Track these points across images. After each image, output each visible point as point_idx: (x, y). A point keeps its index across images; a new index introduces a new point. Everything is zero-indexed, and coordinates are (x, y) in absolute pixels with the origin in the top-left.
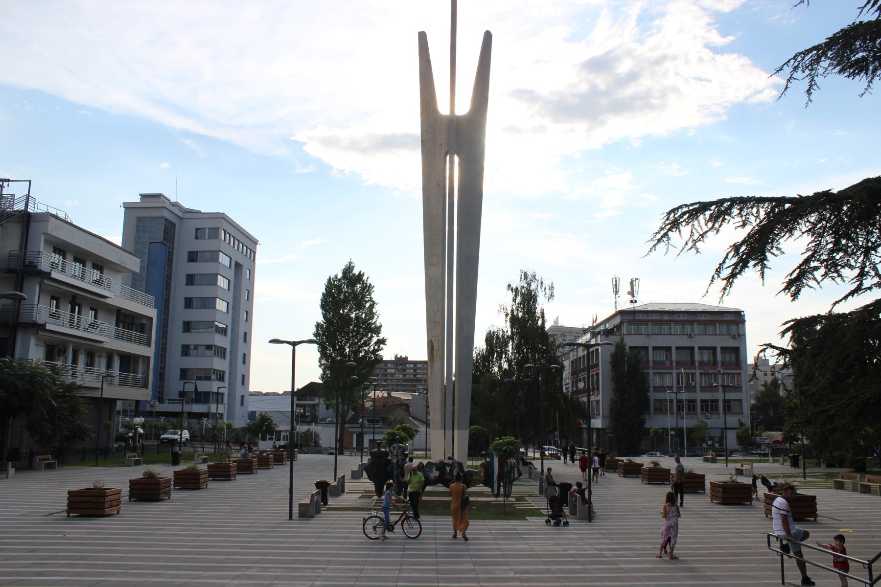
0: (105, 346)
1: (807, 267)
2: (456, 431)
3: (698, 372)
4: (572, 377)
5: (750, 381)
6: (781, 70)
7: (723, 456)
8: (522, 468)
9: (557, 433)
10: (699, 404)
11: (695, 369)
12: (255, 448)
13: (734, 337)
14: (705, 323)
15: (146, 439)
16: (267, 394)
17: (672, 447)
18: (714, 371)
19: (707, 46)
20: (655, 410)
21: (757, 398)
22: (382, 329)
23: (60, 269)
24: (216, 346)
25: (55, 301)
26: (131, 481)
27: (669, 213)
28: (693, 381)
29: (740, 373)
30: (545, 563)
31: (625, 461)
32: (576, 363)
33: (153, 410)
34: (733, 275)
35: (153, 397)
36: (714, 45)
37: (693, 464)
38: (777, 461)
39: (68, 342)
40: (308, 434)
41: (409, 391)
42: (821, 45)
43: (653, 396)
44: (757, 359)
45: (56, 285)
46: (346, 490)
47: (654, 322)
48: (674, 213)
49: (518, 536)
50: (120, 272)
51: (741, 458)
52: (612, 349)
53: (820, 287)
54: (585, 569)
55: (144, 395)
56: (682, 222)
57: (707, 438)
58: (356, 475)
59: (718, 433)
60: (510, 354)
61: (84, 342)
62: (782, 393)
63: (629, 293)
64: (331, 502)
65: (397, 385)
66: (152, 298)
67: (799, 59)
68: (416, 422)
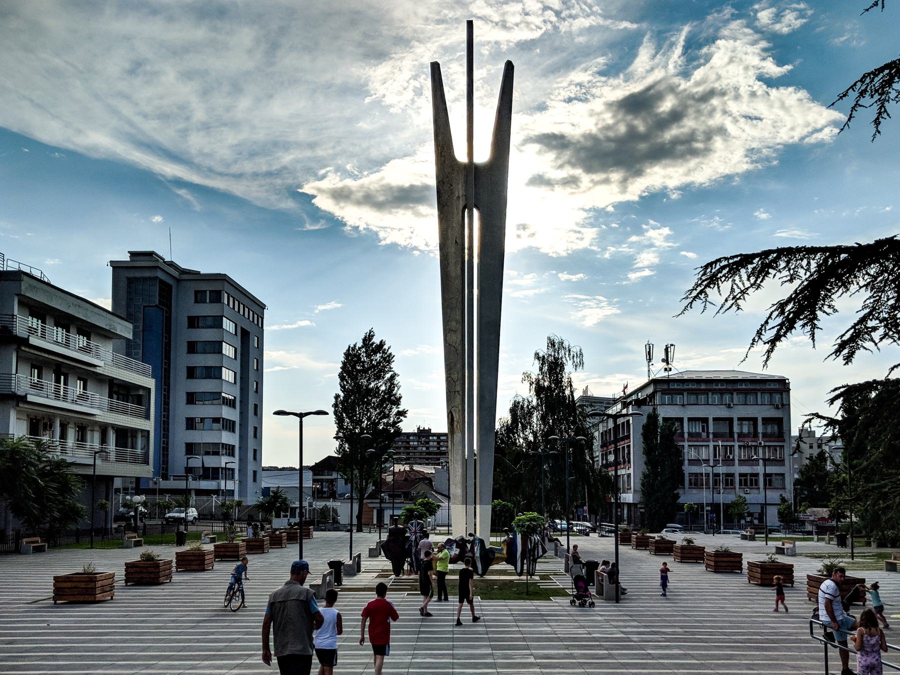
0: (97, 419)
1: (863, 326)
2: (478, 507)
3: (736, 444)
4: (602, 450)
5: (793, 455)
6: (845, 96)
7: (763, 533)
8: (548, 545)
9: (586, 508)
10: (761, 479)
11: (734, 441)
12: (268, 526)
13: (777, 408)
14: (746, 392)
15: (150, 518)
16: (284, 469)
17: (707, 523)
18: (754, 444)
19: (760, 78)
20: (691, 484)
21: (801, 472)
22: (402, 400)
23: (39, 334)
24: (223, 419)
25: (36, 370)
26: (126, 564)
27: (706, 267)
28: (731, 453)
29: (783, 446)
30: (567, 647)
31: (656, 538)
32: (606, 435)
33: (157, 487)
34: (777, 338)
35: (156, 473)
36: (767, 76)
37: (730, 541)
38: (823, 540)
39: (54, 415)
40: (324, 511)
41: (432, 464)
42: (894, 62)
43: (688, 469)
44: (801, 431)
45: (36, 352)
46: (362, 569)
47: (691, 392)
48: (712, 267)
49: (542, 618)
50: (110, 338)
51: (783, 536)
52: (644, 420)
53: (878, 349)
54: (610, 654)
55: (146, 471)
56: (721, 277)
57: (746, 514)
58: (373, 554)
59: (758, 509)
60: (535, 426)
61: (73, 415)
62: (829, 467)
63: (663, 360)
64: (347, 582)
65: (420, 458)
66: (149, 367)
67: (868, 80)
68: (439, 497)
